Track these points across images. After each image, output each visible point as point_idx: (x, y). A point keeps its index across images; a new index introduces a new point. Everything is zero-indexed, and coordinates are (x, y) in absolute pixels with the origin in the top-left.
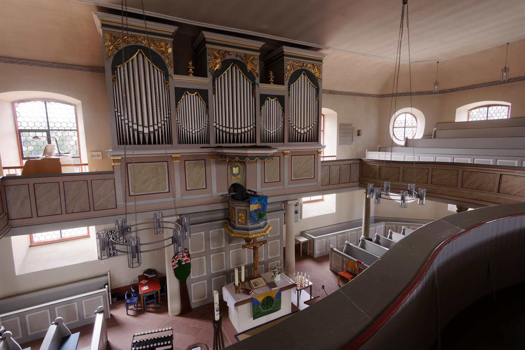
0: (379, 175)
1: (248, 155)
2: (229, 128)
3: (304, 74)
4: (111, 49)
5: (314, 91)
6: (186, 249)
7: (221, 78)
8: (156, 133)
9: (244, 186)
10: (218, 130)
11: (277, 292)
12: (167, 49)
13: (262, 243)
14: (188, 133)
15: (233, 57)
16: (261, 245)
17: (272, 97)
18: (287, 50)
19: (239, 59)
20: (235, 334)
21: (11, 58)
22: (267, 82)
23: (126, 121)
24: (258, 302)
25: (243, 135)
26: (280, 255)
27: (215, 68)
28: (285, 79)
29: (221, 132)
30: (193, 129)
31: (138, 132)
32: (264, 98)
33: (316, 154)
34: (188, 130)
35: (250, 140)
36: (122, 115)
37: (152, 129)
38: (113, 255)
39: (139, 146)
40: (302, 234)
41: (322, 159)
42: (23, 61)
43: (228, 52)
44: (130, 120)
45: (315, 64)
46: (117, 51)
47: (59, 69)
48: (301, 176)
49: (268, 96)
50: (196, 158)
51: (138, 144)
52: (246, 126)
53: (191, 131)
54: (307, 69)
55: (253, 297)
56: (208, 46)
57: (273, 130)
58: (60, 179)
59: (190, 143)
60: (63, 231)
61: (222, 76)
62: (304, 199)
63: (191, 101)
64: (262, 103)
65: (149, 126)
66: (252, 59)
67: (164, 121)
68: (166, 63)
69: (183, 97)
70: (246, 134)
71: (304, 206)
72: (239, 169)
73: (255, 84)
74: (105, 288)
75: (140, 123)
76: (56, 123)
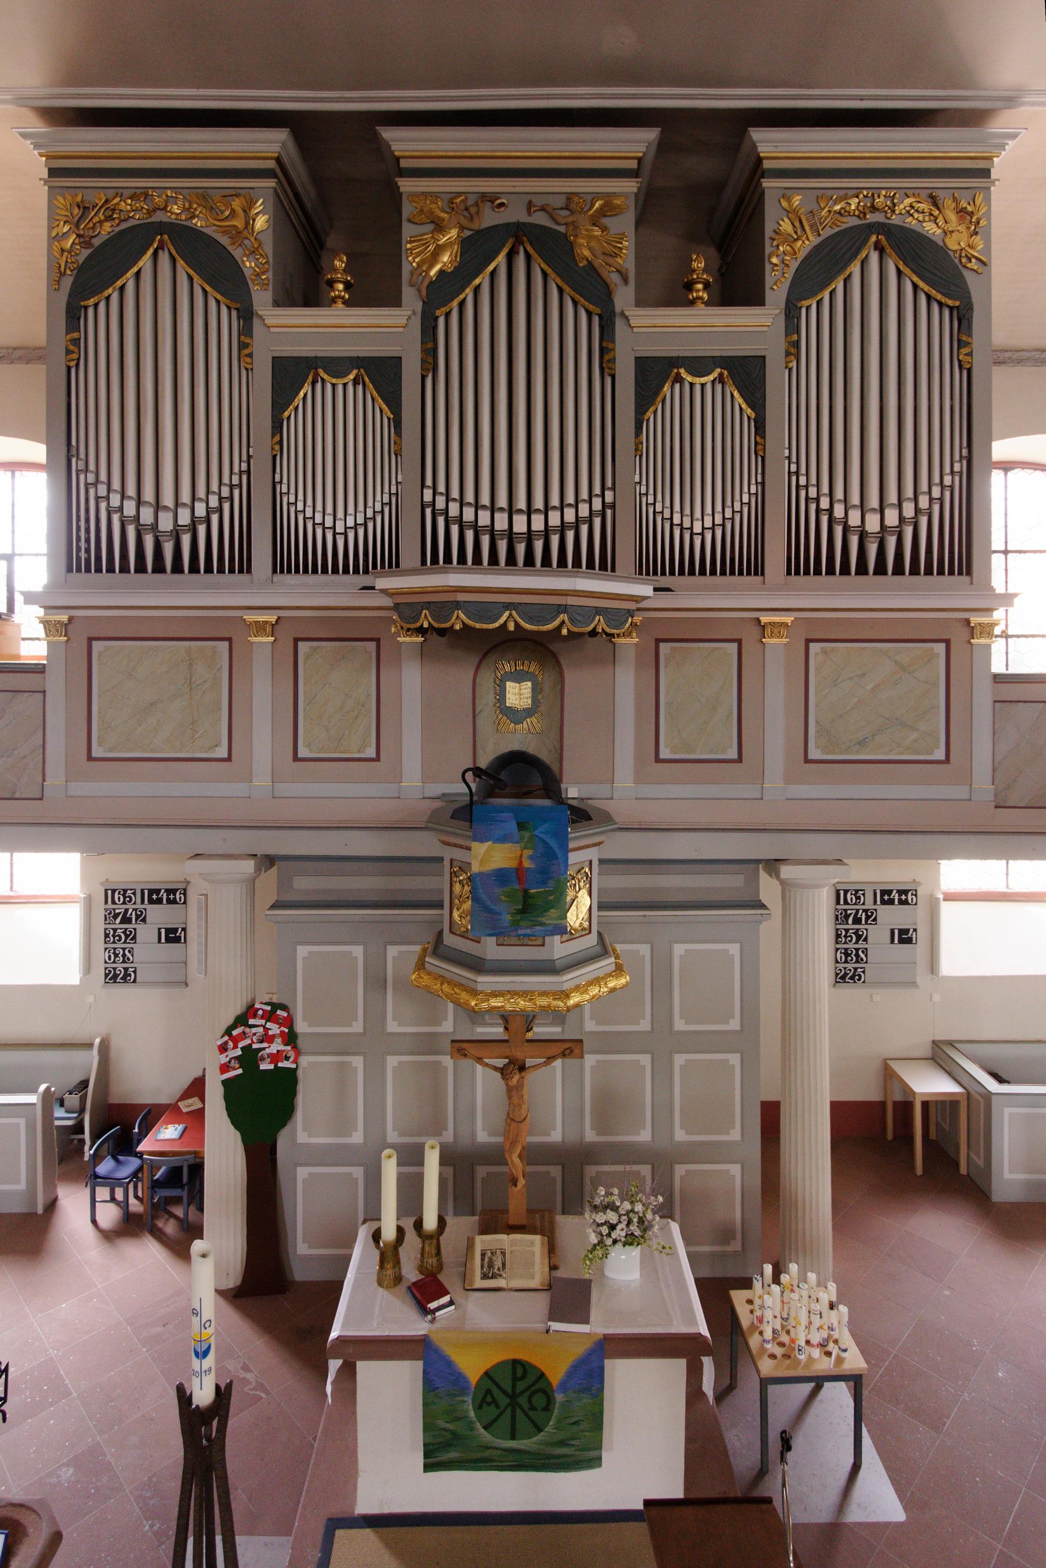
0: (754, 209)
1: (461, 597)
3: (879, 248)
5: (941, 323)
6: (284, 1008)
7: (462, 305)
8: (202, 529)
9: (555, 767)
10: (441, 521)
11: (579, 1350)
13: (557, 1049)
14: (319, 532)
15: (515, 214)
16: (551, 1059)
19: (540, 219)
20: (336, 1510)
22: (678, 295)
23: (102, 490)
24: (458, 1379)
25: (555, 540)
26: (741, 1132)
27: (431, 266)
28: (769, 280)
29: (455, 529)
31: (846, 529)
33: (958, 637)
36: (803, 470)
37: (184, 517)
38: (124, 978)
40: (939, 1056)
46: (86, 253)
48: (862, 743)
49: (674, 362)
50: (341, 631)
54: (895, 220)
55: (437, 1340)
56: (407, 185)
61: (469, 292)
62: (956, 873)
63: (337, 412)
64: (647, 394)
66: (602, 212)
67: (232, 487)
68: (248, 273)
69: (307, 388)
70: (570, 535)
72: (534, 689)
74: (34, 1091)
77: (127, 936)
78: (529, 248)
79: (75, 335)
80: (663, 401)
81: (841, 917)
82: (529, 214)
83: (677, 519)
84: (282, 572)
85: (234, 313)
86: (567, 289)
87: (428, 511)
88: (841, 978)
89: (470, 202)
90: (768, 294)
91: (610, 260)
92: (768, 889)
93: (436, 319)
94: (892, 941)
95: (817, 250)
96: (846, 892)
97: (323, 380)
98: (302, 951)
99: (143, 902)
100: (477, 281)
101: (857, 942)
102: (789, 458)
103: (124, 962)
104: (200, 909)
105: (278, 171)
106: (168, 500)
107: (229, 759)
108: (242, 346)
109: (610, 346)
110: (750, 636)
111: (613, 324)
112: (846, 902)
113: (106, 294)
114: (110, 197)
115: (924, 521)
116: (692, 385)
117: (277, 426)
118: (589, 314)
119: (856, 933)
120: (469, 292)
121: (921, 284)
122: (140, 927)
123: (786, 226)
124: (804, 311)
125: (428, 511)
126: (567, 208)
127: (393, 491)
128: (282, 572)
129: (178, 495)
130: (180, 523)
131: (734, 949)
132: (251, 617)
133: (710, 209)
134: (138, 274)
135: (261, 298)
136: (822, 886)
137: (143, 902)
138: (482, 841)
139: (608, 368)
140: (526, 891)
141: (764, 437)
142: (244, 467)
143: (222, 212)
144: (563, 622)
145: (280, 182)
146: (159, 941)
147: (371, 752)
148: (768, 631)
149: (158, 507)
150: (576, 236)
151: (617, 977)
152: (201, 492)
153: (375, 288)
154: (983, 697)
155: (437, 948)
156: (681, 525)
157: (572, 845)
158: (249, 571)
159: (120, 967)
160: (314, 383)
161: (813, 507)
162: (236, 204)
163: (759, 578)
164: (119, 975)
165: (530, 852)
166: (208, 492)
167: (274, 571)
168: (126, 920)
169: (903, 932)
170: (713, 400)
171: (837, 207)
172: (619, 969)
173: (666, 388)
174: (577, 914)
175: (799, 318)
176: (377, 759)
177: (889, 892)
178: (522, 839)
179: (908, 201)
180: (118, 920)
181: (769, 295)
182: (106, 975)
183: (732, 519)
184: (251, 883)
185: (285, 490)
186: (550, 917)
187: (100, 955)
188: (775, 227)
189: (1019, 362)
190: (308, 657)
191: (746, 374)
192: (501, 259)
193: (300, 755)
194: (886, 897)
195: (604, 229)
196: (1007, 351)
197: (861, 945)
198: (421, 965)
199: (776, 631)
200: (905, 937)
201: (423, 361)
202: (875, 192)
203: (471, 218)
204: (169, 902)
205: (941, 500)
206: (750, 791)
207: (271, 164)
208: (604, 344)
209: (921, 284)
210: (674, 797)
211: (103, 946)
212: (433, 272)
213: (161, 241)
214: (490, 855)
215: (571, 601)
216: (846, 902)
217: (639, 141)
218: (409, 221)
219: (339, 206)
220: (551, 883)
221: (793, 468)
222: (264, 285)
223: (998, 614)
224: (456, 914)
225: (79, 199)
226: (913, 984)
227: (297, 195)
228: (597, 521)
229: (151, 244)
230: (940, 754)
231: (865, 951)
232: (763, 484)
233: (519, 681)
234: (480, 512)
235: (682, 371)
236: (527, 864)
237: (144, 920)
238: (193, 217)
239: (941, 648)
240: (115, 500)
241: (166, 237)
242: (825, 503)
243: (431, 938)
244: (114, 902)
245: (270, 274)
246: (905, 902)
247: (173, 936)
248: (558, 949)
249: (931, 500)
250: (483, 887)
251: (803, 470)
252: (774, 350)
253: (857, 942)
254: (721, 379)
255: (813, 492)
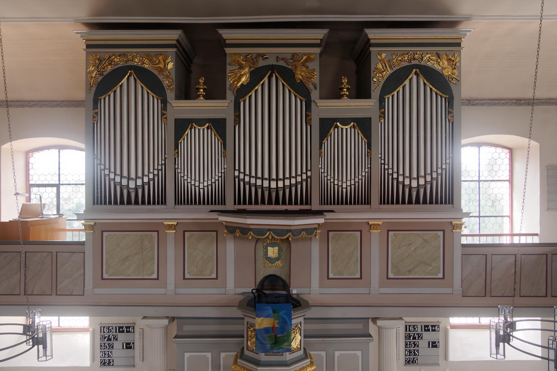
1: (251, 227)
2: (263, 179)
3: (416, 73)
4: (94, 76)
7: (250, 97)
9: (287, 281)
10: (242, 183)
12: (166, 65)
17: (345, 122)
18: (373, 34)
19: (282, 63)
21: (22, 101)
25: (287, 191)
28: (373, 88)
30: (344, 180)
31: (404, 186)
32: (327, 125)
33: (448, 230)
34: (193, 183)
35: (294, 201)
36: (387, 163)
37: (139, 182)
38: (108, 364)
39: (122, 206)
41: (464, 241)
42: (32, 103)
43: (262, 55)
44: (395, 170)
45: (441, 53)
46: (101, 78)
47: (68, 108)
49: (336, 120)
50: (202, 228)
51: (120, 204)
52: (293, 174)
53: (197, 184)
56: (228, 50)
57: (347, 182)
58: (24, 248)
59: (195, 203)
60: (62, 318)
61: (253, 93)
62: (454, 320)
63: (200, 140)
65: (284, 178)
66: (306, 61)
67: (158, 170)
68: (165, 85)
69: (188, 131)
70: (293, 189)
71: (452, 333)
73: (310, 101)
75: (401, 172)
76: (55, 176)
77: (109, 346)
78: (277, 75)
79: (96, 111)
80: (331, 135)
81: (408, 337)
82: (277, 61)
83: (336, 182)
84: (178, 204)
85: (160, 101)
86: (292, 91)
87: (237, 180)
88: (410, 362)
89: (254, 57)
90: (372, 93)
91: (310, 80)
92: (372, 329)
93: (240, 103)
94: (429, 347)
95: (391, 75)
96: (410, 326)
97: (195, 128)
98: (187, 355)
99: (116, 332)
100: (256, 88)
101: (414, 347)
102: (381, 158)
103: (108, 357)
104: (140, 335)
105: (178, 45)
106: (133, 175)
107: (158, 279)
108: (163, 115)
109: (309, 114)
110: (365, 229)
111: (311, 105)
112: (410, 331)
113: (109, 94)
114: (111, 56)
115: (435, 182)
116: (342, 129)
117: (176, 147)
118: (301, 101)
119: (414, 343)
120: (253, 93)
121: (433, 89)
122: (115, 343)
123: (380, 66)
124: (387, 99)
125: (237, 180)
126: (292, 59)
127: (223, 171)
128: (178, 204)
129: (137, 173)
130: (138, 184)
131: (359, 353)
132: (166, 223)
133: (349, 58)
134: (121, 86)
135: (170, 95)
136: (394, 328)
137: (116, 332)
138: (259, 317)
139: (308, 121)
140: (276, 336)
141: (370, 150)
142: (163, 162)
143: (155, 61)
144: (290, 236)
145: (178, 49)
146: (123, 348)
147: (214, 276)
148: (372, 227)
149: (129, 178)
150: (296, 70)
151: (311, 366)
152: (146, 173)
153: (215, 92)
154: (458, 253)
155: (241, 355)
156: (338, 184)
157: (293, 317)
158: (165, 204)
159: (107, 359)
160: (191, 129)
161: (390, 177)
162: (160, 58)
163: (369, 206)
164: (106, 363)
165: (277, 321)
166: (149, 172)
167: (175, 204)
168: (109, 339)
169: (434, 343)
170: (349, 134)
171: (400, 58)
172: (312, 363)
173: (332, 130)
174: (295, 344)
175: (385, 102)
176: (217, 278)
177: (428, 326)
178: (274, 316)
179: (428, 56)
180: (106, 340)
181: (373, 94)
182: (101, 363)
183: (358, 182)
184: (166, 328)
185: (179, 171)
186: (285, 346)
187: (98, 354)
188: (375, 66)
189: (482, 104)
190: (189, 238)
191: (364, 125)
192: (266, 79)
193: (186, 277)
194: (426, 328)
195: (307, 67)
196: (477, 100)
197: (416, 348)
198: (235, 362)
199: (375, 227)
200: (434, 345)
201: (235, 120)
202: (415, 53)
203: (254, 64)
204: (127, 332)
205: (442, 174)
206: (366, 291)
207: (175, 42)
208: (307, 113)
209: (433, 89)
210: (334, 293)
211: (99, 350)
212: (238, 85)
213: (131, 73)
214: (263, 322)
215: (293, 228)
216: (410, 331)
217: (319, 34)
218: (229, 64)
219: (201, 60)
220: (285, 333)
221: (383, 162)
222: (171, 90)
223: (464, 220)
224: (249, 343)
225: (98, 57)
226: (438, 364)
227: (183, 49)
228: (304, 183)
229: (127, 74)
230: (441, 276)
231: (418, 351)
232: (370, 168)
233: (273, 246)
234: (257, 180)
235: (338, 123)
236: (276, 326)
237: (117, 340)
238: (144, 63)
239: (441, 233)
240: (112, 176)
241: (132, 71)
242: (395, 176)
243: (239, 350)
244: (104, 332)
245: (174, 86)
246: (434, 330)
247: (129, 346)
248: (288, 357)
249: (437, 174)
250: (261, 334)
251: (387, 163)
252: (375, 116)
253: (414, 347)
254: (354, 126)
255: (390, 171)
